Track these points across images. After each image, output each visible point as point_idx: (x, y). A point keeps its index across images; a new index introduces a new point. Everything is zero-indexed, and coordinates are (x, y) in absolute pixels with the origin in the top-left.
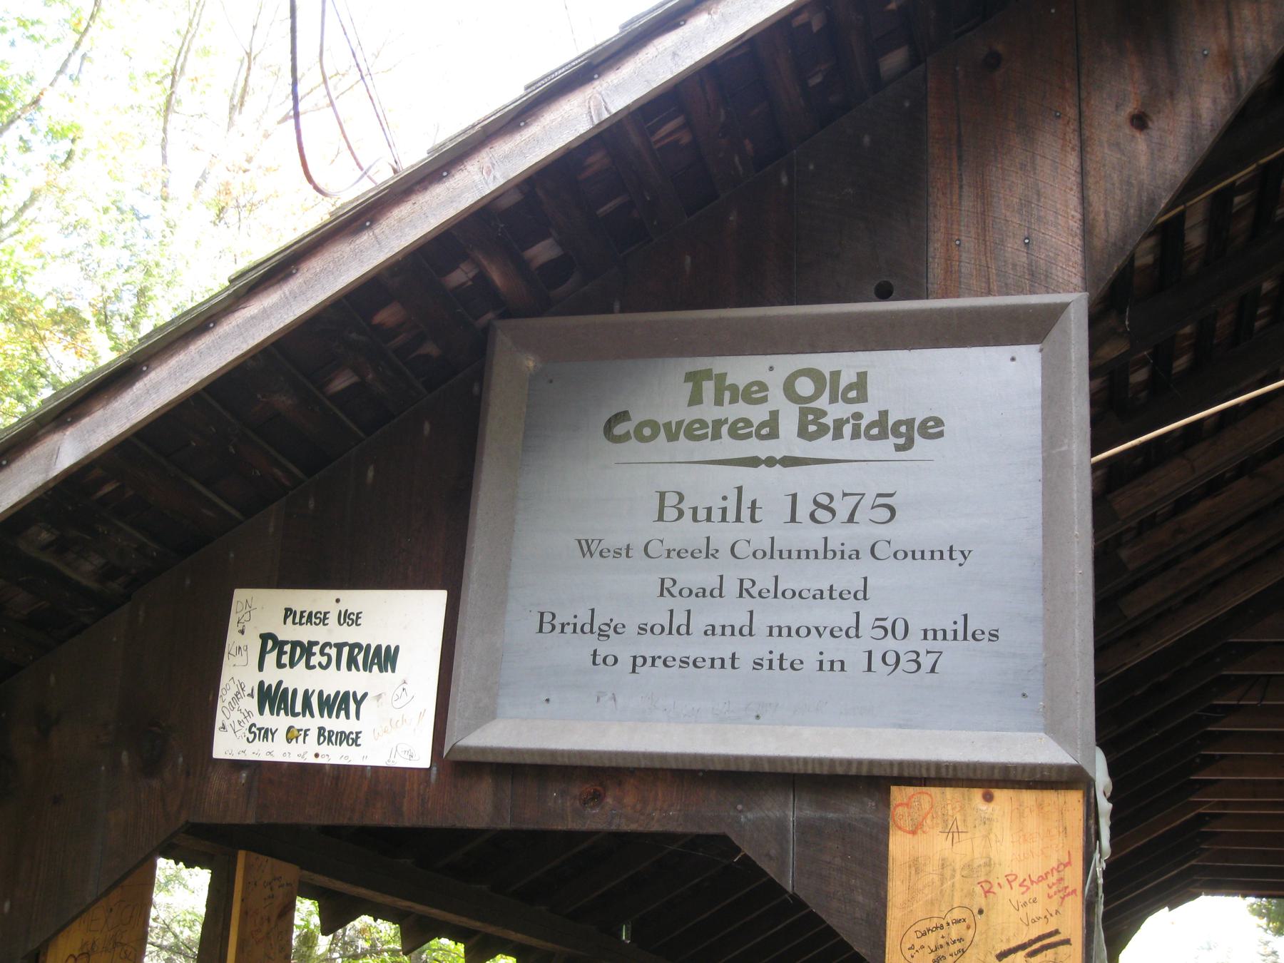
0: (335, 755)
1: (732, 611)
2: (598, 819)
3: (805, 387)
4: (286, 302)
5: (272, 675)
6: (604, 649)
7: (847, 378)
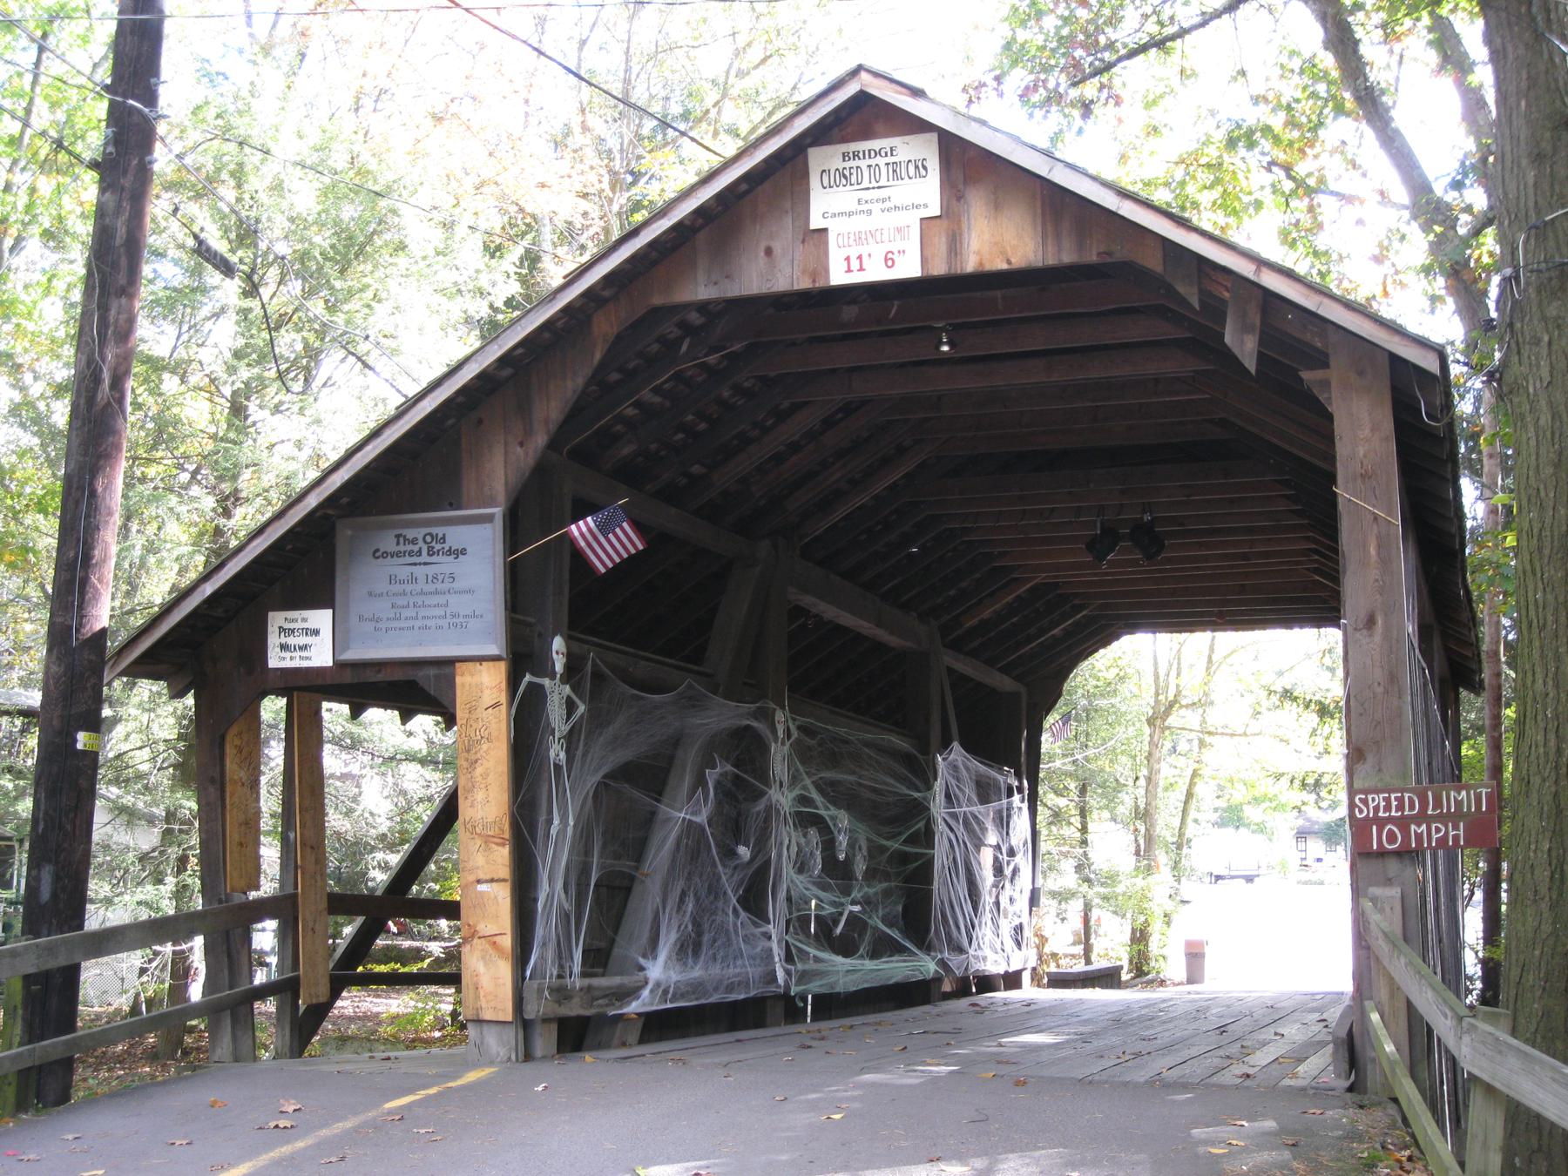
0: (305, 664)
1: (410, 612)
2: (380, 677)
3: (428, 539)
4: (265, 540)
5: (283, 640)
6: (379, 625)
7: (440, 536)
